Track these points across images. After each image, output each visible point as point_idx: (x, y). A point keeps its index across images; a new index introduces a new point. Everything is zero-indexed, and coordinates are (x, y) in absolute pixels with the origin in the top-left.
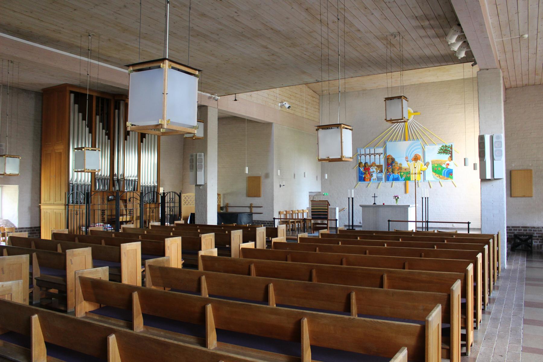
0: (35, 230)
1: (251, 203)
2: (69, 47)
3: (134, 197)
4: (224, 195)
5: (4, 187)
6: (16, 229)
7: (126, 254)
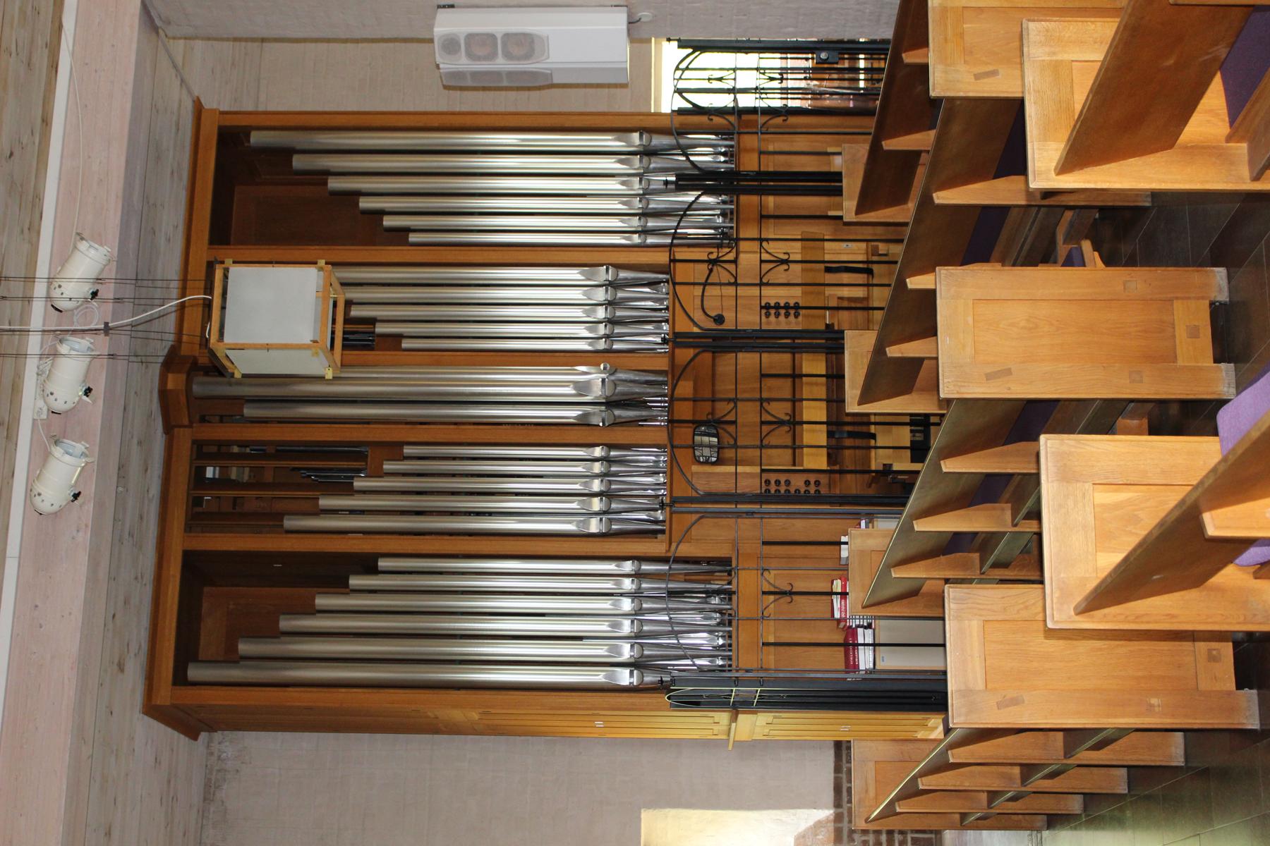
6: (838, 818)
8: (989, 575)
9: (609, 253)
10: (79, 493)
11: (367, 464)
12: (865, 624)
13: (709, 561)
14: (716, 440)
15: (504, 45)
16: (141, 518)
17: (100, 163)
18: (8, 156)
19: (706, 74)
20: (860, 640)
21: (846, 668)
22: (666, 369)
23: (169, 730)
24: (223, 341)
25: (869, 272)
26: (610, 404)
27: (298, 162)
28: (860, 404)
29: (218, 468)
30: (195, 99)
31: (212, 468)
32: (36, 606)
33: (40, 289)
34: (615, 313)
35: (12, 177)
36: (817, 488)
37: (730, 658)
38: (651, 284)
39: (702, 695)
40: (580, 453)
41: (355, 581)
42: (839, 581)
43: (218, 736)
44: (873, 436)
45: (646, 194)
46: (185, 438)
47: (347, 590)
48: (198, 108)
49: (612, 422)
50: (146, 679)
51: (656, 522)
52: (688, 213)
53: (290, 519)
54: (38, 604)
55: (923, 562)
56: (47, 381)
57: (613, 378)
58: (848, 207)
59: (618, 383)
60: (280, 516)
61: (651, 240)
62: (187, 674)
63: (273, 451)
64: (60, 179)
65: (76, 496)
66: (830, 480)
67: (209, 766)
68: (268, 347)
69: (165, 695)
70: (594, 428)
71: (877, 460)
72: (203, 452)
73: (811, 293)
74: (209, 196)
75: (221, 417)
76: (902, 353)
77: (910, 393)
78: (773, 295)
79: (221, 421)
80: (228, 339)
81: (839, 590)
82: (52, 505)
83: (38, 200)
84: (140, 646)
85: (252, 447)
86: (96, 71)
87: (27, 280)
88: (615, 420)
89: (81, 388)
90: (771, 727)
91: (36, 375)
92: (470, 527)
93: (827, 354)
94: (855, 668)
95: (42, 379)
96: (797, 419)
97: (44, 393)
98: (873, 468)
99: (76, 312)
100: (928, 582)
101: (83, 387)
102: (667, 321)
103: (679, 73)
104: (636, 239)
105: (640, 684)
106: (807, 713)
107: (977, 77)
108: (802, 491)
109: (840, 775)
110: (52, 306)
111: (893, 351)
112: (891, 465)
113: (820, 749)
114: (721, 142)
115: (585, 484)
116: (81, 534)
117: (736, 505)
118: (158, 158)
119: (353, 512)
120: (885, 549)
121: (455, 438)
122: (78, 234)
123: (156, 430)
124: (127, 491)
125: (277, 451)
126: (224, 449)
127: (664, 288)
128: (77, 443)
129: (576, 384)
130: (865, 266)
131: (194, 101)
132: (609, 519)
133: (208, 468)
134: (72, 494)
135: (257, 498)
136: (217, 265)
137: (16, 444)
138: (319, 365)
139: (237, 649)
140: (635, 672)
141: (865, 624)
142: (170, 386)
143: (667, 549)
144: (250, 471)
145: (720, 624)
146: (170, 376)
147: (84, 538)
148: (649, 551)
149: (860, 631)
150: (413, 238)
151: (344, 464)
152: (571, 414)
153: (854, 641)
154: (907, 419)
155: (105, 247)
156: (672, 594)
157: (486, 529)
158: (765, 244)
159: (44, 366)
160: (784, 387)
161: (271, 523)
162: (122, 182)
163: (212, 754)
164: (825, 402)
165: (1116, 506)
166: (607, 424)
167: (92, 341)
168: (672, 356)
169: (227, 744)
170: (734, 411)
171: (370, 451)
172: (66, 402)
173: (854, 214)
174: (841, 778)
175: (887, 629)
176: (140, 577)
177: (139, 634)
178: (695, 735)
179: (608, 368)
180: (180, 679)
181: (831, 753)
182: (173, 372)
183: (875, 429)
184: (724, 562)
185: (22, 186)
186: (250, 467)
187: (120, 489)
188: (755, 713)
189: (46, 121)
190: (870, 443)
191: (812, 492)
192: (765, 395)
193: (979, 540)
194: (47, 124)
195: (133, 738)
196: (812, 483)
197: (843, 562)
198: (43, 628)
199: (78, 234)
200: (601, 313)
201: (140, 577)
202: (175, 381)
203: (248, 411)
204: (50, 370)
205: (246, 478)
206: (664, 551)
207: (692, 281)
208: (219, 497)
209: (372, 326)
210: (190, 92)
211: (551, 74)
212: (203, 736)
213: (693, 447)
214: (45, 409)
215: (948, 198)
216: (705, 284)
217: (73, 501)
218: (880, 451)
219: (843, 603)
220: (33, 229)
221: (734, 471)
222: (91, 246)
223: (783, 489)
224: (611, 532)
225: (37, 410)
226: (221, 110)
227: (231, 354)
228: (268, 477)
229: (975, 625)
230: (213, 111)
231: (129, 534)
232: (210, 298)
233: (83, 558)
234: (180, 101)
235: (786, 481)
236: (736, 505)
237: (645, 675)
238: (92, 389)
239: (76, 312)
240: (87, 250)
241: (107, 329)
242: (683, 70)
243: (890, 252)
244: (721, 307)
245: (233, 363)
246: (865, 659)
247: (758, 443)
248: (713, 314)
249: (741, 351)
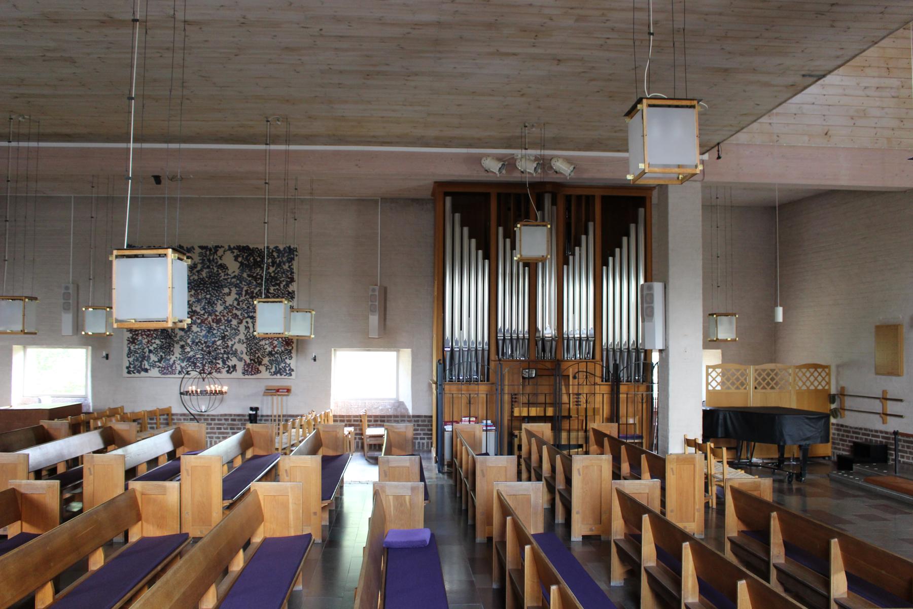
0: (210, 420)
1: (884, 388)
2: (309, 139)
3: (588, 371)
4: (838, 366)
5: (400, 352)
6: (409, 416)
7: (190, 472)
14: (534, 376)
15: (649, 307)
41: (480, 252)
61: (605, 353)
81: (471, 420)
96: (530, 405)
107: (578, 470)
115: (521, 331)
165: (405, 501)
216: (587, 372)
229: (408, 464)
230: (651, 194)
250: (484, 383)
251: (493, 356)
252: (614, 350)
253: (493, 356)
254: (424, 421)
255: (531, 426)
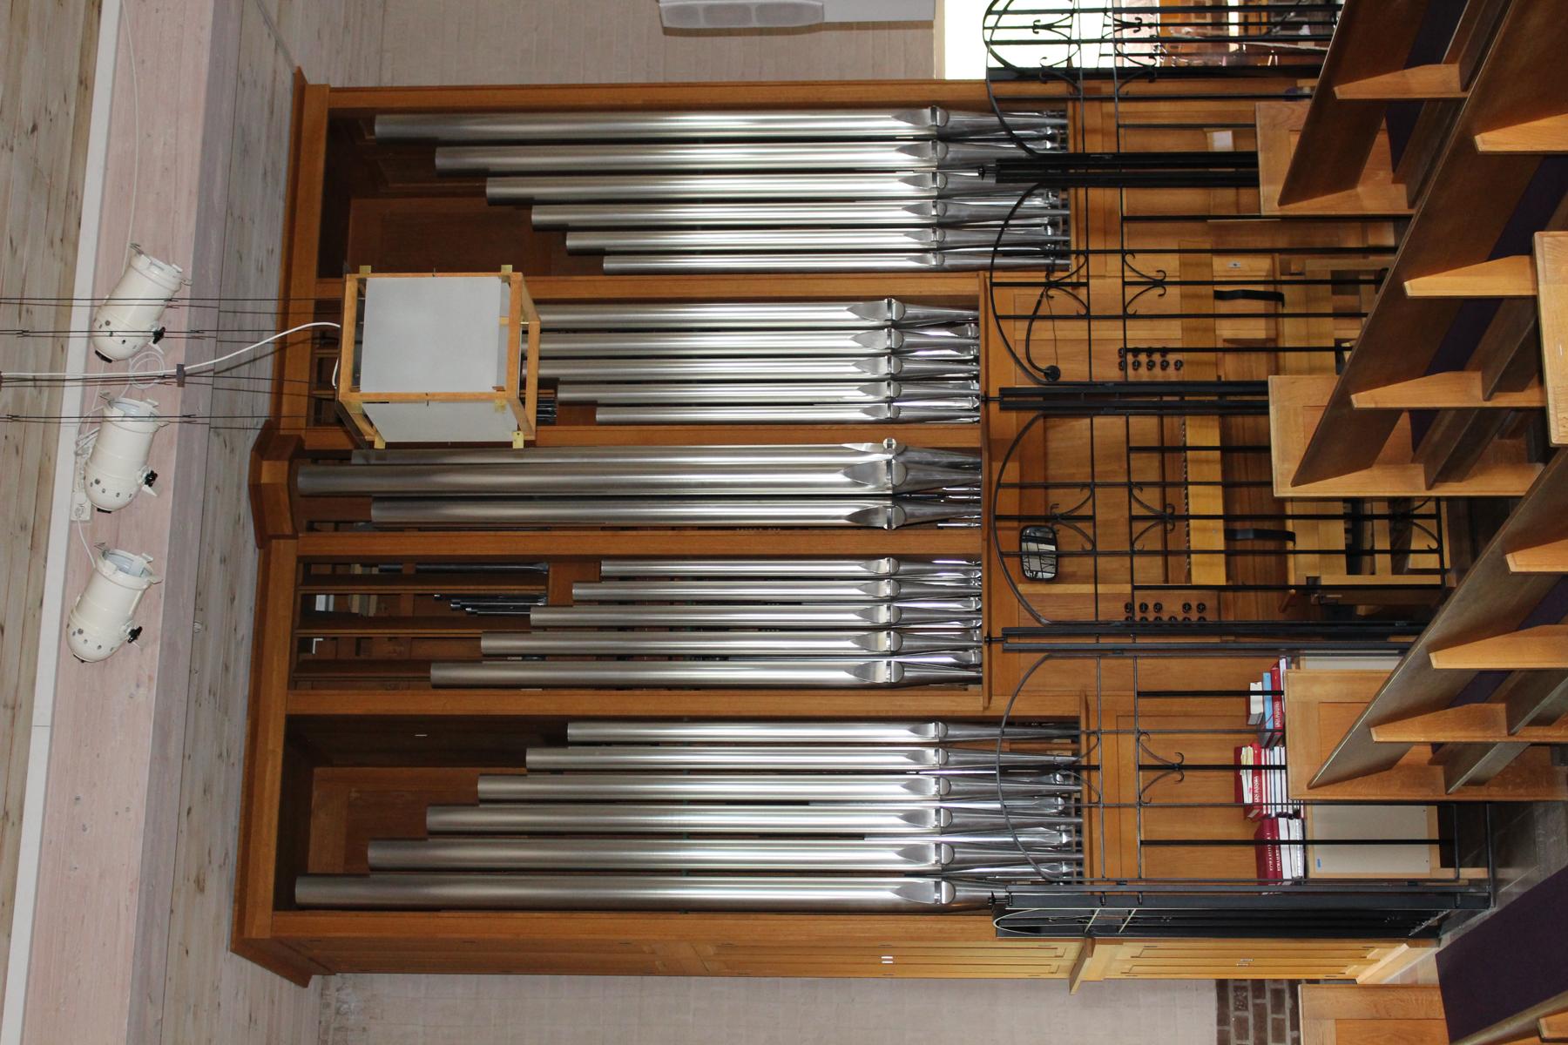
8: (1522, 737)
9: (889, 282)
10: (140, 629)
11: (547, 589)
12: (1291, 812)
13: (1041, 722)
16: (227, 668)
17: (165, 144)
18: (30, 130)
19: (1029, 20)
20: (1283, 836)
21: (1259, 876)
22: (979, 445)
23: (268, 973)
24: (359, 390)
25: (1278, 297)
26: (897, 497)
27: (443, 161)
28: (1295, 483)
29: (332, 597)
30: (295, 70)
31: (323, 597)
32: (77, 799)
33: (79, 318)
34: (902, 366)
35: (36, 161)
36: (1202, 615)
37: (1079, 863)
38: (950, 324)
39: (1048, 919)
40: (855, 568)
41: (534, 757)
42: (1250, 749)
43: (336, 980)
44: (1291, 536)
45: (943, 196)
46: (287, 553)
47: (523, 770)
48: (300, 86)
49: (901, 524)
50: (234, 902)
51: (967, 667)
52: (1011, 222)
53: (439, 668)
54: (80, 795)
55: (1419, 718)
56: (89, 463)
57: (901, 459)
58: (1269, 195)
59: (909, 465)
60: (426, 664)
62: (294, 891)
63: (412, 572)
64: (106, 168)
65: (135, 634)
66: (1219, 603)
67: (323, 1024)
68: (427, 399)
69: (263, 922)
70: (876, 531)
71: (1299, 570)
72: (312, 573)
73: (1196, 329)
74: (317, 208)
75: (337, 523)
76: (1376, 403)
77: (1370, 466)
78: (1140, 334)
79: (336, 530)
80: (367, 387)
81: (1251, 762)
82: (100, 647)
83: (74, 197)
84: (227, 854)
85: (380, 566)
86: (157, 11)
87: (61, 302)
88: (906, 520)
89: (140, 473)
90: (1139, 962)
91: (73, 456)
92: (647, 677)
93: (1221, 416)
94: (1276, 877)
95: (84, 461)
97: (87, 481)
98: (1292, 581)
99: (131, 362)
100: (1414, 748)
101: (144, 471)
102: (976, 378)
103: (992, 20)
104: (932, 261)
105: (950, 902)
106: (1179, 941)
108: (1180, 618)
109: (1226, 1028)
110: (97, 353)
111: (1362, 400)
112: (1316, 579)
113: (1197, 990)
114: (1048, 121)
116: (142, 691)
117: (1098, 640)
118: (245, 152)
119: (527, 657)
120: (1368, 700)
121: (675, 549)
122: (135, 246)
123: (246, 542)
124: (206, 629)
125: (418, 571)
126: (340, 570)
127: (970, 330)
128: (135, 554)
129: (849, 470)
130: (1271, 288)
131: (294, 74)
132: (900, 663)
133: (318, 597)
134: (129, 630)
135: (390, 639)
136: (348, 275)
137: (46, 558)
138: (508, 427)
139: (367, 855)
140: (944, 884)
141: (1291, 812)
142: (265, 478)
143: (986, 705)
144: (379, 603)
145: (1065, 813)
146: (266, 465)
147: (147, 696)
148: (959, 708)
149: (1282, 821)
150: (609, 264)
151: (516, 589)
152: (842, 511)
153: (1273, 836)
154: (1339, 509)
155: (174, 266)
156: (1006, 771)
157: (695, 680)
158: (1128, 258)
159: (85, 441)
160: (1147, 469)
161: (410, 675)
162: (197, 169)
163: (328, 1005)
164: (1220, 487)
166: (894, 526)
167: (156, 404)
168: (985, 424)
169: (350, 990)
170: (1091, 501)
171: (551, 570)
172: (118, 495)
173: (1276, 204)
174: (1229, 1032)
175: (1321, 822)
176: (225, 754)
177: (224, 836)
178: (1022, 973)
179: (894, 446)
180: (285, 900)
181: (1213, 995)
182: (268, 459)
183: (1294, 525)
184: (1067, 725)
185: (51, 176)
186: (378, 594)
187: (197, 626)
188: (1120, 943)
189: (86, 83)
190: (1285, 546)
191: (1151, 619)
192: (1135, 479)
193: (1510, 684)
194: (86, 88)
195: (217, 987)
196: (1151, 607)
197: (1252, 721)
198: (88, 831)
199: (135, 246)
200: (884, 367)
201: (225, 754)
202: (272, 473)
203: (377, 514)
204: (94, 447)
205: (372, 612)
206: (981, 709)
207: (1012, 314)
208: (336, 638)
209: (552, 391)
210: (288, 59)
211: (823, 7)
212: (316, 980)
213: (1021, 555)
214: (88, 506)
215: (1502, 144)
216: (1033, 318)
217: (130, 641)
218: (1301, 557)
219: (1256, 781)
220: (68, 241)
221: (1093, 591)
222: (151, 263)
223: (1151, 616)
224: (902, 682)
225: (75, 506)
226: (332, 86)
227: (371, 410)
228: (406, 608)
231: (210, 691)
232: (339, 326)
233: (146, 727)
234: (275, 72)
235: (1156, 605)
236: (1098, 640)
237: (957, 888)
238: (156, 475)
239: (131, 362)
240: (148, 268)
241: (181, 377)
242: (1000, 13)
243: (1307, 269)
244: (1054, 356)
245: (372, 424)
246: (1291, 864)
247: (1127, 548)
248: (1043, 366)
249: (1099, 415)
250: (1087, 863)
251: (970, 703)
252: (942, 225)
253: (970, 703)
254: (1242, 1024)
255: (1284, 458)
